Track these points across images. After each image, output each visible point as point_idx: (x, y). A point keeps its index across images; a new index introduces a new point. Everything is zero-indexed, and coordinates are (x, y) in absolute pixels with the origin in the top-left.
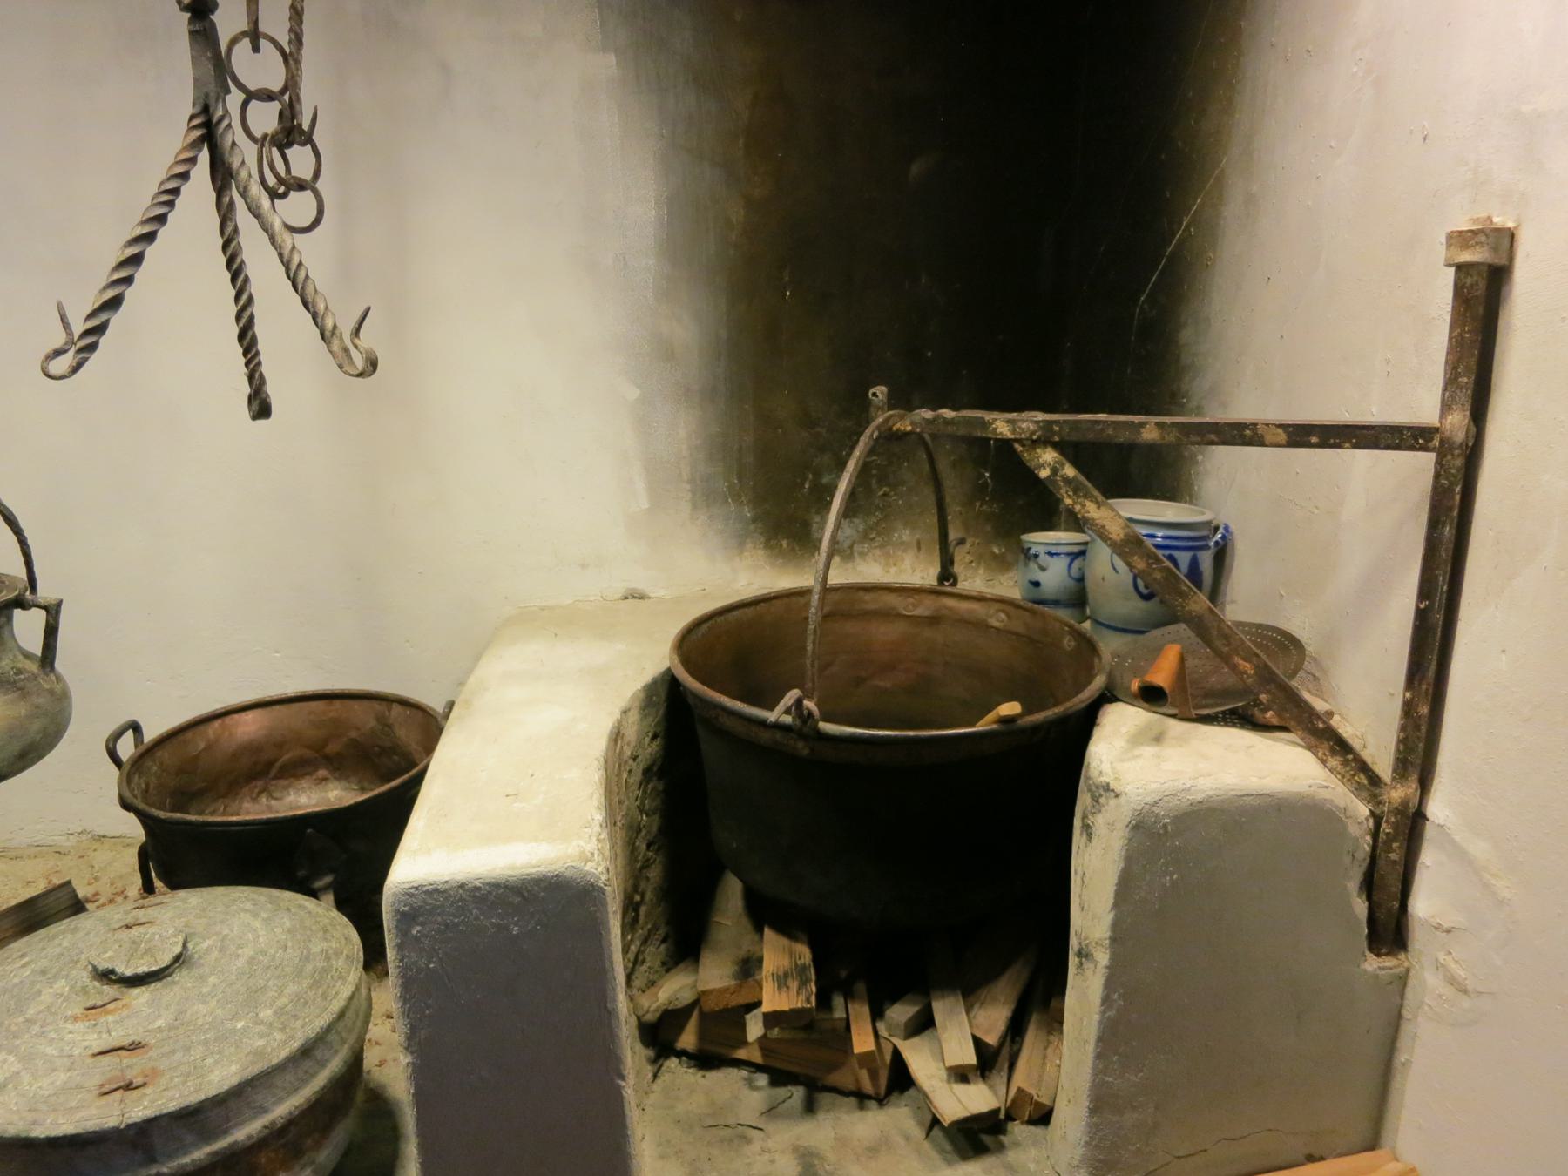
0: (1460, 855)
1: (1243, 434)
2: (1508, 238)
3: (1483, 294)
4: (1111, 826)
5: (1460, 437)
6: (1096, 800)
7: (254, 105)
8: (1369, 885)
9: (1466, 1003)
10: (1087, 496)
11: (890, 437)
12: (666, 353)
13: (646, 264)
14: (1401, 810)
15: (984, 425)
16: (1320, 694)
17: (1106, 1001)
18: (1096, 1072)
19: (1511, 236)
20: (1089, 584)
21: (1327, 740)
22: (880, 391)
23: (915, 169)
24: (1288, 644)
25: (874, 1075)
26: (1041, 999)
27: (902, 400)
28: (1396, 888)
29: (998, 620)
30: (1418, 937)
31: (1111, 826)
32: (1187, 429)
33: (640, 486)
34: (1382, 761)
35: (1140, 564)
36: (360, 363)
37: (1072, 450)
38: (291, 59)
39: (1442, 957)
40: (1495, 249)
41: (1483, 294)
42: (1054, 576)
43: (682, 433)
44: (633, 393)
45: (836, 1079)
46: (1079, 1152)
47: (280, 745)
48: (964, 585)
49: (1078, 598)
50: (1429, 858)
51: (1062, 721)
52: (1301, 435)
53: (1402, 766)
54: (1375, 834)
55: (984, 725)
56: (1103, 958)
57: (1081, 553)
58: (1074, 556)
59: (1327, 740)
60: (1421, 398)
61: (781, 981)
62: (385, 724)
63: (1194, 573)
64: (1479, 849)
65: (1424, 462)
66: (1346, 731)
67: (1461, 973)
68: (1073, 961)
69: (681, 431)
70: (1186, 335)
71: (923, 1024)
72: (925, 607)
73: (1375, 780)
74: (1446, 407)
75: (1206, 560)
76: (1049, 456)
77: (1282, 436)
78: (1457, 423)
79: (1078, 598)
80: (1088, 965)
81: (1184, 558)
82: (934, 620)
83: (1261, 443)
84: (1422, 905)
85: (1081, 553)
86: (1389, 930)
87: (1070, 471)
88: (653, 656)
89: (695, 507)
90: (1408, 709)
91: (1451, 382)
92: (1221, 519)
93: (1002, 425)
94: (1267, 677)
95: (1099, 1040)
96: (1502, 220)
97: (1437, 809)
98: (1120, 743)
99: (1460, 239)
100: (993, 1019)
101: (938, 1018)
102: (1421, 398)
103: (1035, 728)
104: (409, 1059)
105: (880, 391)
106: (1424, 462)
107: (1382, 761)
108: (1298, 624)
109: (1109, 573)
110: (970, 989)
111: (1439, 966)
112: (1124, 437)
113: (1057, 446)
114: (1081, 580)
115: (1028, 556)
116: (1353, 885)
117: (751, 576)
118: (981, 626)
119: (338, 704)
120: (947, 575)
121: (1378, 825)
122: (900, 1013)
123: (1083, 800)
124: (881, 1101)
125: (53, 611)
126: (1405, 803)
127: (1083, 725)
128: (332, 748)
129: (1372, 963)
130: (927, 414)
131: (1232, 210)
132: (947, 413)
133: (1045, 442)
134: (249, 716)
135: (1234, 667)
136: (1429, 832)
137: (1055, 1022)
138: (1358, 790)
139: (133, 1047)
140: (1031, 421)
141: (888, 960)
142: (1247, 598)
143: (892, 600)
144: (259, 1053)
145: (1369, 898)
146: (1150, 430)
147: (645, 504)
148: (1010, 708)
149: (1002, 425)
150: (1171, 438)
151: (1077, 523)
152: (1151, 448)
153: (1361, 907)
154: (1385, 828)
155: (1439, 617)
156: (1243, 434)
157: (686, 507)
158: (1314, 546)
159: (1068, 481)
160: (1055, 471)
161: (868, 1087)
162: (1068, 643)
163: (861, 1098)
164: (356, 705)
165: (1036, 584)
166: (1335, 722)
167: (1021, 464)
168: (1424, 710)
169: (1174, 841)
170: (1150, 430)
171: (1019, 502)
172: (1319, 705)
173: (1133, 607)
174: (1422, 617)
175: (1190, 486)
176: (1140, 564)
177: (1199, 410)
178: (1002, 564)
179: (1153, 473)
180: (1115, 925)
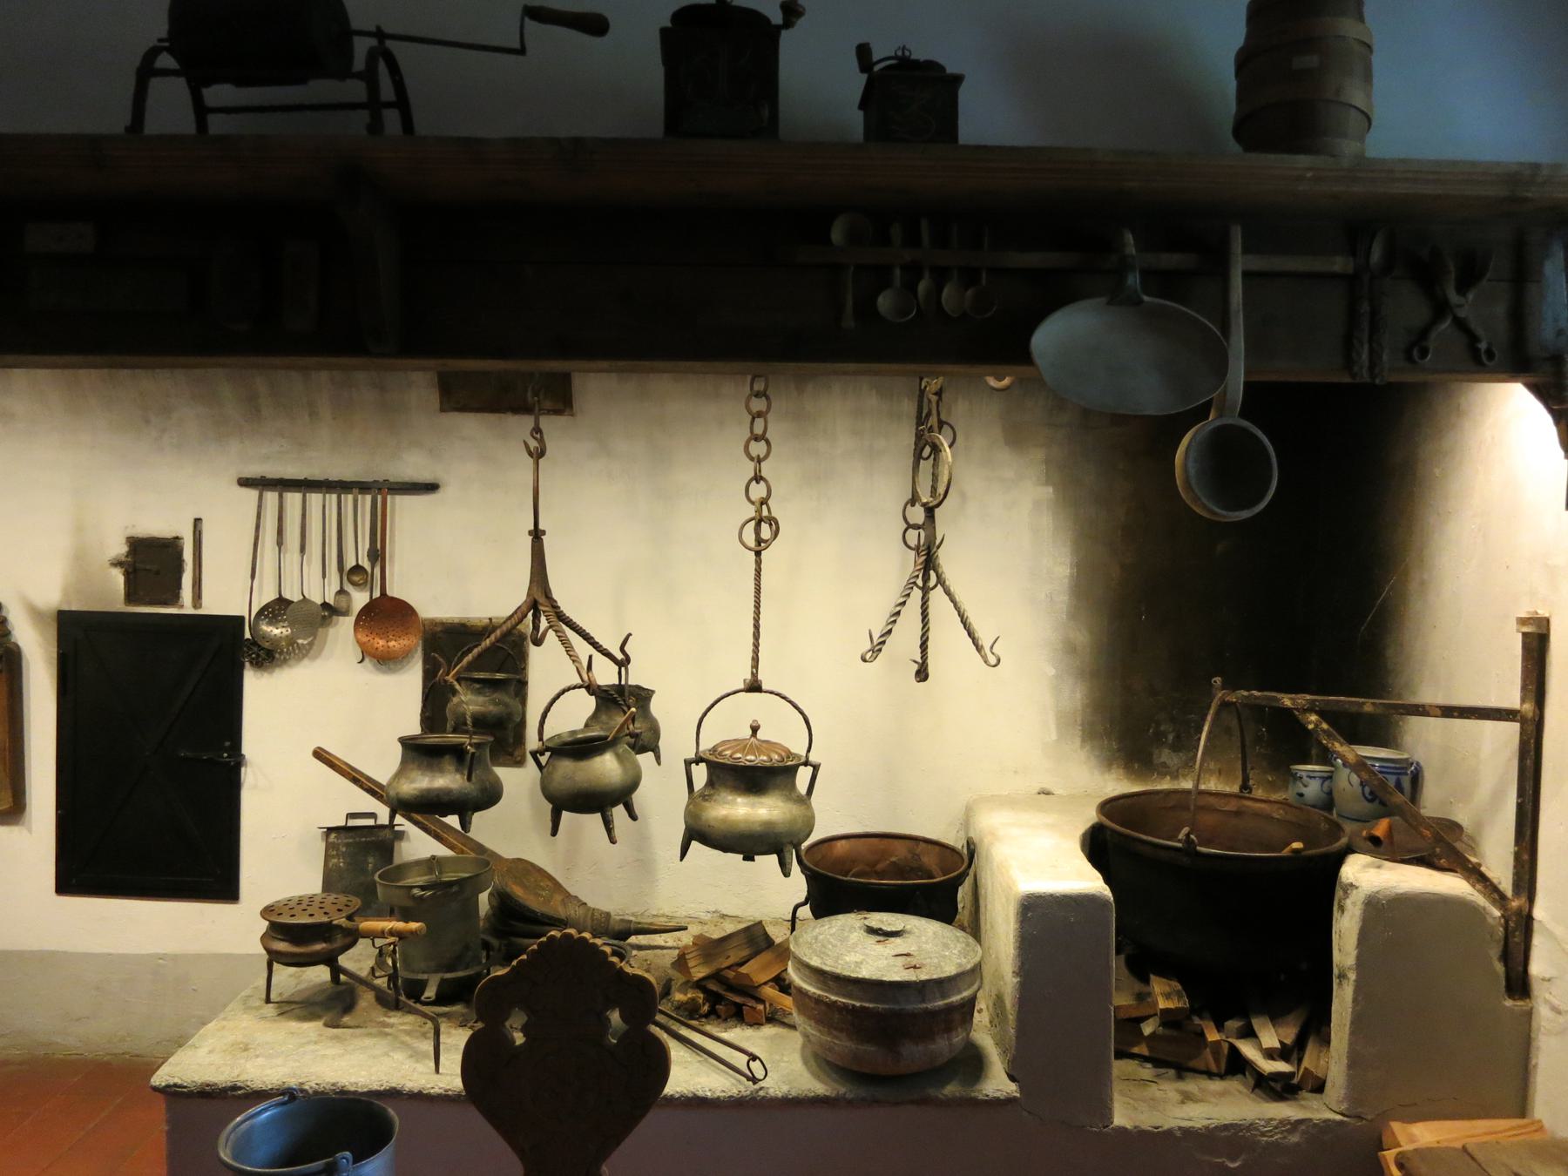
0: (1550, 934)
1: (1421, 710)
2: (1545, 623)
3: (1536, 646)
4: (1354, 904)
5: (1530, 715)
6: (1346, 892)
7: (910, 531)
8: (1505, 957)
9: (1561, 1019)
10: (1335, 739)
11: (1225, 705)
12: (1070, 649)
13: (1063, 600)
14: (1519, 911)
15: (1278, 700)
16: (1475, 855)
17: (1355, 1000)
18: (1351, 1044)
19: (1548, 620)
20: (1336, 795)
21: (1476, 875)
22: (1218, 680)
23: (1220, 548)
24: (1455, 827)
25: (1217, 1061)
26: (1316, 1025)
27: (1231, 685)
28: (1521, 957)
29: (1278, 813)
30: (1538, 989)
31: (1354, 904)
32: (1396, 707)
33: (1053, 727)
34: (1506, 886)
35: (1365, 776)
36: (993, 660)
37: (1323, 714)
38: (930, 511)
39: (1547, 996)
40: (1539, 627)
41: (1536, 646)
42: (1312, 790)
43: (1078, 695)
44: (1051, 671)
45: (1192, 1064)
46: (1343, 1092)
47: (854, 862)
48: (1259, 793)
49: (1328, 803)
50: (1537, 941)
51: (1325, 856)
52: (1449, 712)
53: (1517, 886)
54: (1506, 928)
55: (1285, 852)
56: (1352, 976)
57: (1329, 777)
58: (1324, 779)
59: (1476, 875)
60: (1511, 696)
61: (1167, 996)
62: (916, 857)
63: (1399, 786)
64: (1558, 931)
65: (1514, 728)
66: (1490, 874)
67: (1556, 1002)
68: (1335, 982)
69: (1075, 696)
70: (1390, 652)
71: (1249, 1033)
72: (1232, 806)
73: (1503, 897)
74: (1523, 701)
75: (1406, 782)
76: (1313, 718)
77: (1439, 712)
78: (1528, 708)
79: (1328, 803)
80: (1345, 982)
81: (1392, 780)
82: (1238, 813)
83: (1428, 715)
84: (1537, 968)
85: (1329, 777)
86: (1519, 985)
87: (1325, 726)
88: (1090, 816)
89: (1083, 741)
90: (1517, 856)
91: (1524, 688)
92: (1416, 758)
93: (1287, 701)
94: (1438, 839)
95: (1352, 1023)
96: (1543, 613)
97: (1539, 913)
98: (1356, 868)
99: (1522, 621)
100: (1289, 1034)
101: (1256, 1027)
102: (1511, 696)
103: (1310, 859)
104: (1015, 980)
105: (1218, 680)
106: (1514, 728)
107: (1506, 886)
108: (1462, 817)
109: (1347, 783)
110: (1275, 1017)
111: (1547, 1001)
112: (1354, 709)
113: (1317, 713)
114: (1330, 793)
115: (1296, 778)
116: (1494, 952)
117: (1117, 785)
118: (1269, 818)
119: (886, 841)
120: (1245, 786)
121: (1507, 922)
122: (1233, 1024)
123: (1339, 893)
124: (1222, 1077)
125: (816, 768)
126: (1520, 909)
127: (1339, 859)
128: (880, 867)
129: (1509, 1003)
130: (1246, 693)
131: (1413, 586)
132: (1256, 693)
133: (1311, 710)
134: (843, 842)
135: (1421, 834)
136: (1536, 926)
137: (1326, 1041)
138: (1494, 902)
139: (908, 955)
140: (1303, 699)
141: (1227, 993)
142: (1432, 802)
143: (1212, 800)
144: (960, 965)
145: (1506, 965)
146: (1368, 705)
147: (1054, 737)
148: (1297, 845)
149: (1287, 701)
150: (1379, 711)
151: (1326, 757)
152: (1370, 715)
153: (1500, 968)
154: (1512, 924)
155: (1529, 807)
156: (1421, 710)
157: (1078, 741)
158: (1467, 771)
159: (1324, 731)
160: (1316, 726)
161: (1214, 1068)
162: (1324, 826)
163: (1210, 1075)
164: (896, 842)
165: (1301, 795)
166: (1483, 869)
167: (1297, 721)
168: (1526, 857)
169: (1385, 912)
170: (1368, 705)
171: (1287, 744)
172: (1473, 860)
173: (1364, 807)
174: (1520, 807)
175: (1395, 738)
176: (1365, 776)
177: (1400, 696)
178: (1273, 786)
179: (1378, 731)
180: (1358, 958)
